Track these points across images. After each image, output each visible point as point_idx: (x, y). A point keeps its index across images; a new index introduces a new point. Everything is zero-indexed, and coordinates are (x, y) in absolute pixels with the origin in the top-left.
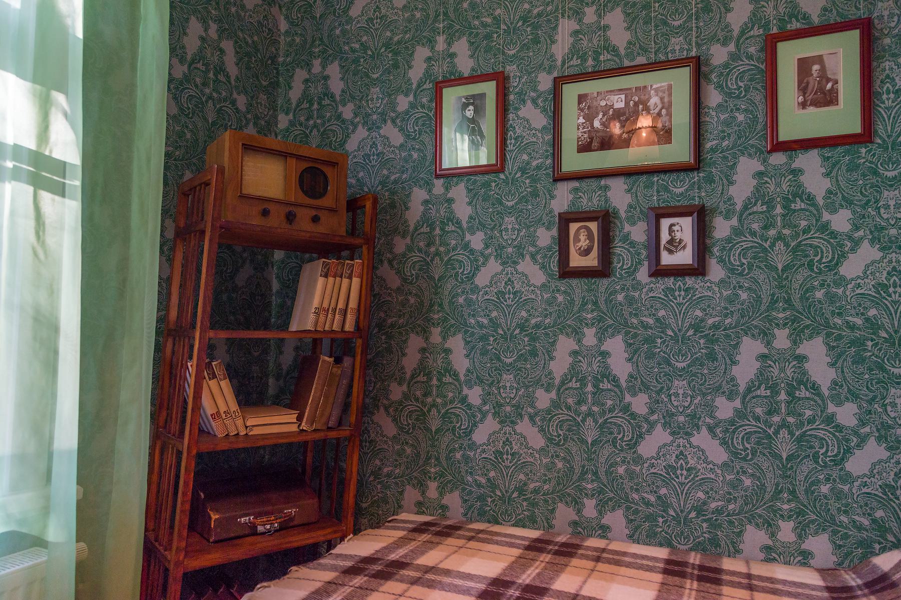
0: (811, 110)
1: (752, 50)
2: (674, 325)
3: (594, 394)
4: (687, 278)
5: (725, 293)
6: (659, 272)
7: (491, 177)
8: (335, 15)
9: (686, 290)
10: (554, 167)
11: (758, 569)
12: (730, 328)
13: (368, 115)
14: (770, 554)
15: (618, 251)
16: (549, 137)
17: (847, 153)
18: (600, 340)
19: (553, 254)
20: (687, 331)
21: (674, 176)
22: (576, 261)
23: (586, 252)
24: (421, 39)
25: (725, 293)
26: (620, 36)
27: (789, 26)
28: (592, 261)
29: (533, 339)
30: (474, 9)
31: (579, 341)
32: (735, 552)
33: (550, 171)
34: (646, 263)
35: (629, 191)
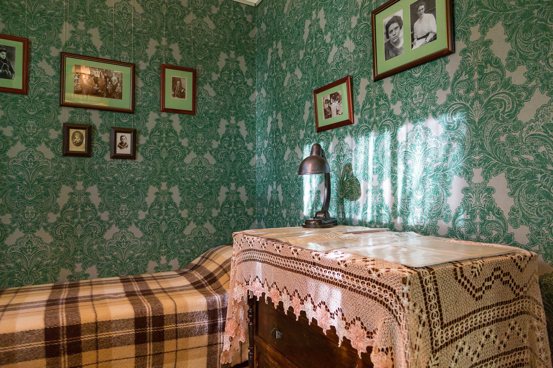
0: (176, 98)
1: (156, 68)
2: (198, 181)
3: (166, 211)
4: (128, 160)
5: (54, 165)
6: (116, 157)
7: (18, 96)
9: (127, 165)
10: (60, 98)
11: (155, 275)
12: (56, 181)
13: (119, 220)
14: (157, 269)
15: (95, 145)
16: (57, 82)
17: (187, 117)
20: (34, 182)
21: (122, 114)
22: (73, 148)
23: (79, 144)
24: (363, 73)
25: (54, 165)
26: (97, 41)
27: (485, 70)
28: (82, 149)
29: (211, 187)
31: (74, 188)
32: (145, 272)
33: (58, 100)
34: (109, 152)
35: (101, 117)
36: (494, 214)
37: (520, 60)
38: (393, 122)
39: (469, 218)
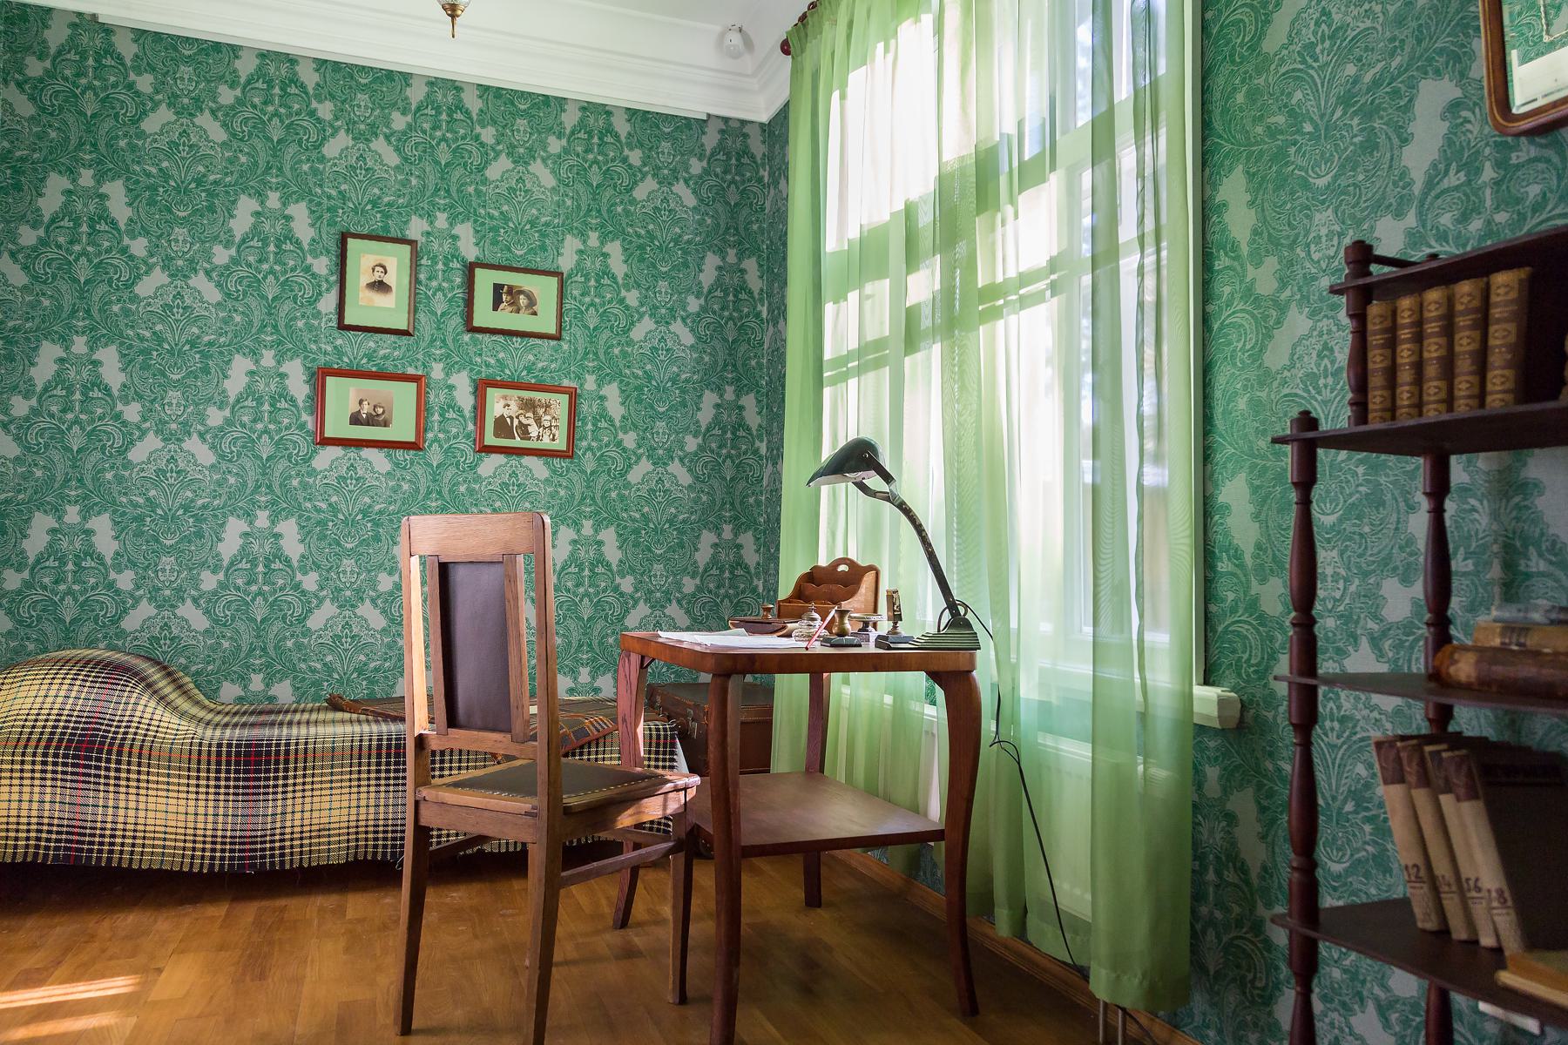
8: (1233, 62)
18: (736, 535)
19: (1417, 640)
24: (1430, 60)
27: (1514, 155)
30: (1254, 101)
36: (1541, 555)
37: (1270, 247)
38: (1253, 316)
39: (1471, 568)
